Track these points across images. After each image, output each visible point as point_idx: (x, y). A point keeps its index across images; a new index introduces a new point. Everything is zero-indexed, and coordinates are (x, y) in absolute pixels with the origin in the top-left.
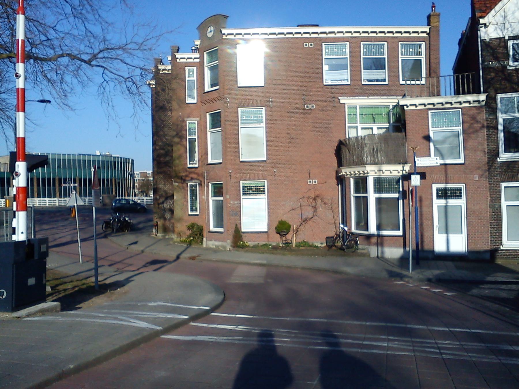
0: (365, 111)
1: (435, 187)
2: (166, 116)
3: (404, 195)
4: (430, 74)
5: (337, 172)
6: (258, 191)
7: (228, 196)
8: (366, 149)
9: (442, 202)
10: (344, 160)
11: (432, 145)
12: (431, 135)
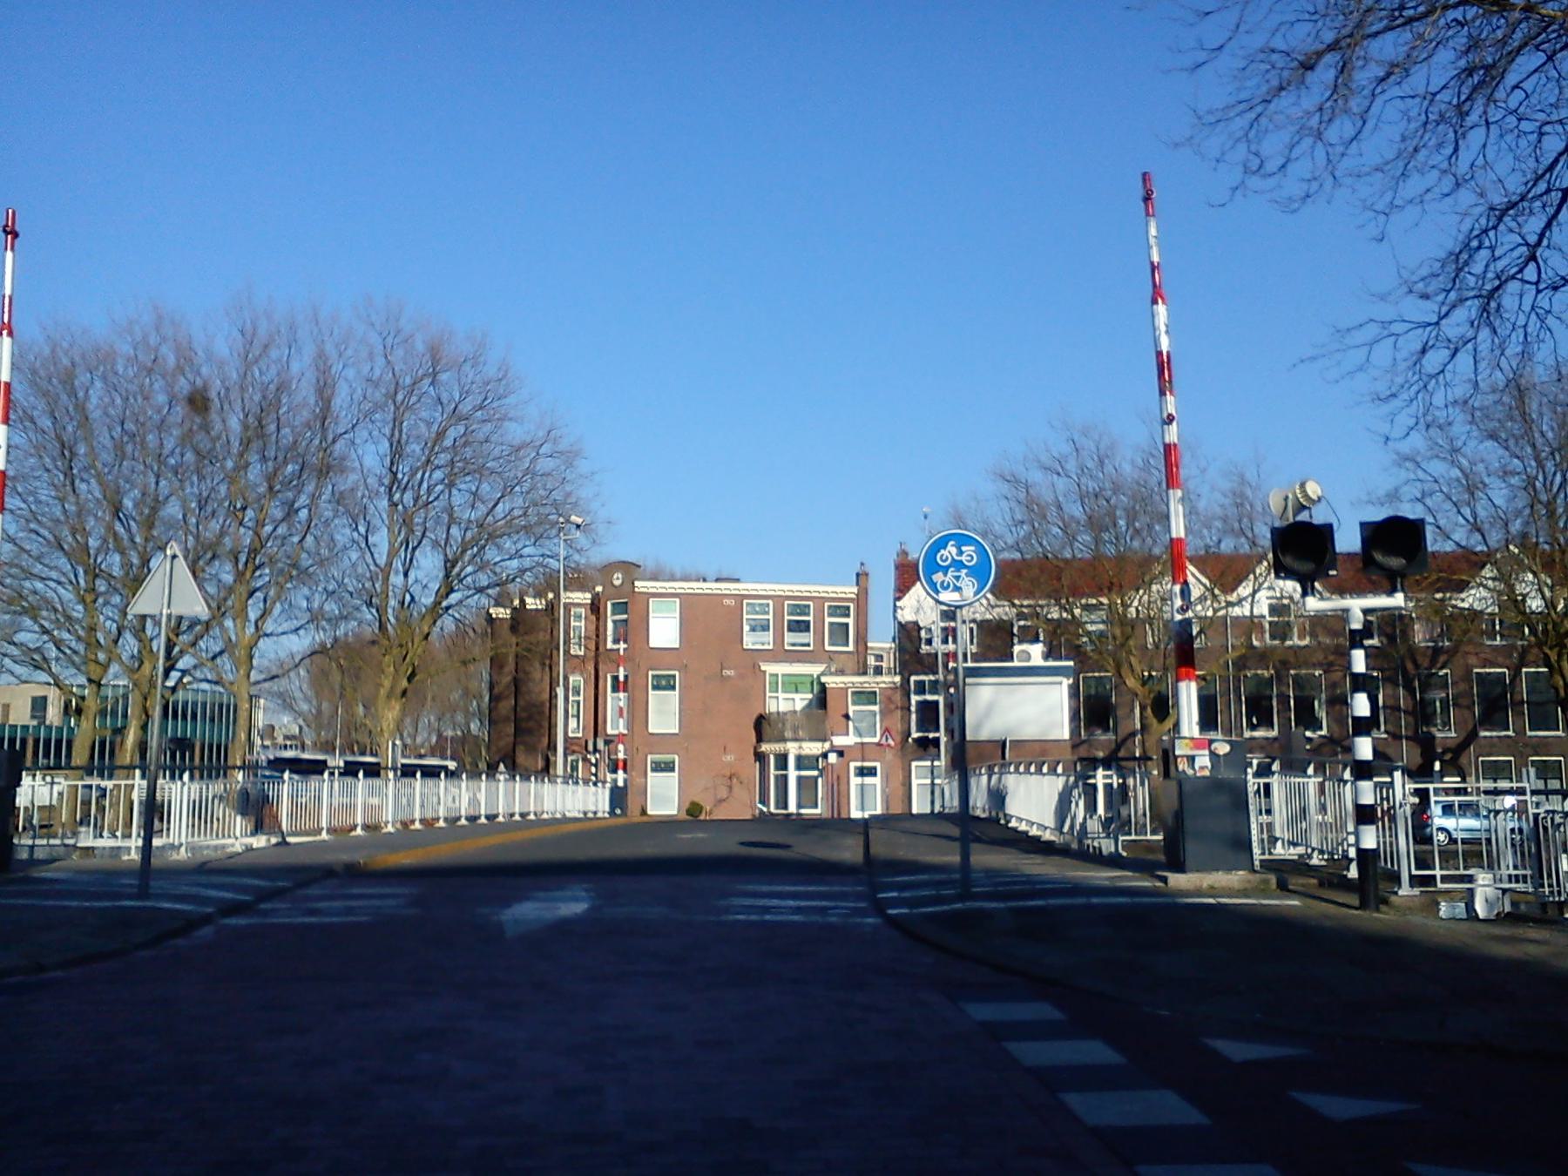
0: (786, 678)
1: (853, 765)
2: (532, 665)
3: (821, 772)
4: (857, 642)
5: (755, 748)
6: (668, 767)
7: (634, 773)
8: (788, 725)
9: (859, 780)
10: (765, 737)
11: (850, 723)
12: (851, 714)
